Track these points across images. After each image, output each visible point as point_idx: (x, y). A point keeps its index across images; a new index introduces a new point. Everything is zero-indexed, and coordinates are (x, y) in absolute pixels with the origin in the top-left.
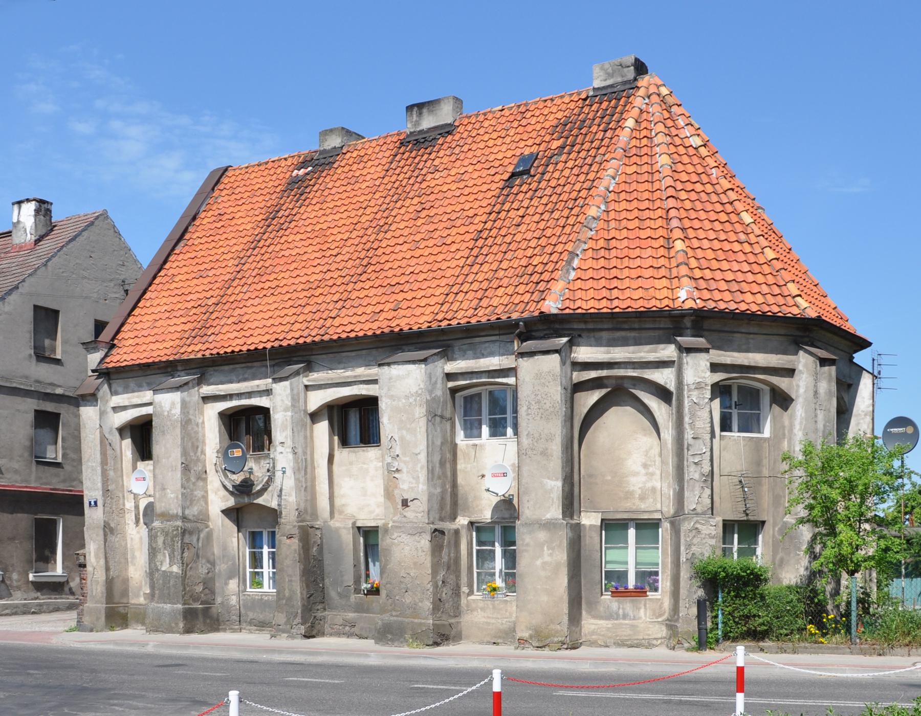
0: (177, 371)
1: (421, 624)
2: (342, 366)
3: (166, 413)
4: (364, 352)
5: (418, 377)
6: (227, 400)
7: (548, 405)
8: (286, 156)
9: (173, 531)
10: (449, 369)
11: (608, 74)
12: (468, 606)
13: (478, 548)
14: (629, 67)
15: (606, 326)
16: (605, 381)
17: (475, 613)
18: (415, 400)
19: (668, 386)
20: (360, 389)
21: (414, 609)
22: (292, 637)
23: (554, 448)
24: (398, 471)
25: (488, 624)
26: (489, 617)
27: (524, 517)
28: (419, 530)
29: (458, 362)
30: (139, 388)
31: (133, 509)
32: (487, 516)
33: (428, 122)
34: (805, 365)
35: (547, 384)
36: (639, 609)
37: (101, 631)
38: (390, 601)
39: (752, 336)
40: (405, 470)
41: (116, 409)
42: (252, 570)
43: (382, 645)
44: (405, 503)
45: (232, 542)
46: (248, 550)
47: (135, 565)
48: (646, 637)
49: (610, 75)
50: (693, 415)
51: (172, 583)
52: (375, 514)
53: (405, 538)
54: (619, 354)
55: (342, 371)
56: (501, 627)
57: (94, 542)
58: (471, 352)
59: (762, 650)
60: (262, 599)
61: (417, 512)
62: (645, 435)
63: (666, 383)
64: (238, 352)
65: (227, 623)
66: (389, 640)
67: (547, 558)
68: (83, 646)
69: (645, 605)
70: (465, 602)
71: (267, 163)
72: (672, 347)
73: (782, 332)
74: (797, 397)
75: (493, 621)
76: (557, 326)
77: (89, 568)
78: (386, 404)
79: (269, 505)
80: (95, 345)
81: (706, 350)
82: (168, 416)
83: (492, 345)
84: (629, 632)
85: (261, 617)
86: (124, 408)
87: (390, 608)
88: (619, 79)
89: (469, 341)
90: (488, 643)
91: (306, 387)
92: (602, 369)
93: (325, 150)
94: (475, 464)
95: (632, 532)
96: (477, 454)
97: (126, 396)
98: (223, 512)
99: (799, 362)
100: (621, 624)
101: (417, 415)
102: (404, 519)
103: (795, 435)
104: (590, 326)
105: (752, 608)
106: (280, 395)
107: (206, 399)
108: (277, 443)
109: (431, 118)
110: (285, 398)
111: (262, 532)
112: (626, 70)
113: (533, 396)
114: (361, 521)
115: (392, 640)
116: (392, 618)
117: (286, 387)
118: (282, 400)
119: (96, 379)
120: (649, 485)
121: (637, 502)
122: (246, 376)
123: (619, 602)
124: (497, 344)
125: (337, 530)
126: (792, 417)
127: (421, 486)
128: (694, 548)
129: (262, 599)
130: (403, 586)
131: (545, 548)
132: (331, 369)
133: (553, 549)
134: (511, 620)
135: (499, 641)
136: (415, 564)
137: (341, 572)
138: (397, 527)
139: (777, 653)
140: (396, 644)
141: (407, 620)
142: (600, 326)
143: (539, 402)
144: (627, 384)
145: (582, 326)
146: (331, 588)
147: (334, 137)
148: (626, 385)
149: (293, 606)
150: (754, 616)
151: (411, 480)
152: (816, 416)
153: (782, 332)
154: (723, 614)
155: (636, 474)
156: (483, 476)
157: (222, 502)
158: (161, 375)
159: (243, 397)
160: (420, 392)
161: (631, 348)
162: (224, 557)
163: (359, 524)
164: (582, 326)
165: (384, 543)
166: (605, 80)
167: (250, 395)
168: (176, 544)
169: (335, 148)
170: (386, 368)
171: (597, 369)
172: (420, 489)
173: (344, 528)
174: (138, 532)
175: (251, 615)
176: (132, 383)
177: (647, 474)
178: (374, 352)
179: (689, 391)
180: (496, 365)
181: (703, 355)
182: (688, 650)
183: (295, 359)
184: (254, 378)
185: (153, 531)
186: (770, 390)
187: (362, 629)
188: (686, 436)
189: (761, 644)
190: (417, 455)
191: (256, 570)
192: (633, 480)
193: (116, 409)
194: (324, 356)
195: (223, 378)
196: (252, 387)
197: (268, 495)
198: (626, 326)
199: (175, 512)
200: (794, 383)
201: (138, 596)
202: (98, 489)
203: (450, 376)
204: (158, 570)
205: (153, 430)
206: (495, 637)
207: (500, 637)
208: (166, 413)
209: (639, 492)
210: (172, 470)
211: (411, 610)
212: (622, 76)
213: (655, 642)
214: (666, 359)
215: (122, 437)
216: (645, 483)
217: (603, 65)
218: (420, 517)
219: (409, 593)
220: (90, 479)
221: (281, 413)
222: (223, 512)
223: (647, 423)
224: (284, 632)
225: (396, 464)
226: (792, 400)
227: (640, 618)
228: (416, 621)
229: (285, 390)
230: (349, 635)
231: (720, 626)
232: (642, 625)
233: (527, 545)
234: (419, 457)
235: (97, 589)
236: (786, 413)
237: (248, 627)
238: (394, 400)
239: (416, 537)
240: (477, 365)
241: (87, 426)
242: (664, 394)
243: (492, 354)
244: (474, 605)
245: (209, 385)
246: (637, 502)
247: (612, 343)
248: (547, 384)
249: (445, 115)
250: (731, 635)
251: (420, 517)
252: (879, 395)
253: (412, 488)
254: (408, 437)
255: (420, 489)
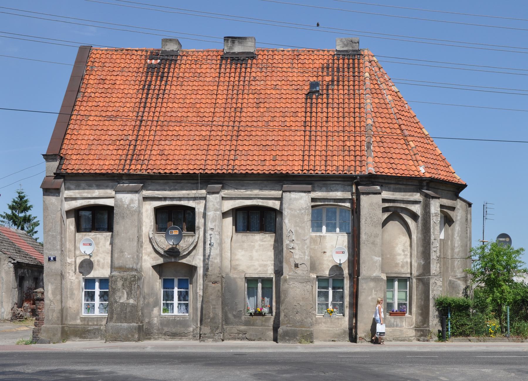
0: (123, 180)
1: (306, 331)
2: (244, 188)
3: (126, 206)
4: (259, 182)
5: (307, 200)
6: (162, 201)
7: (375, 220)
8: (137, 49)
9: (131, 278)
10: (314, 196)
11: (345, 44)
12: (316, 321)
13: (319, 290)
14: (356, 43)
15: (393, 182)
16: (390, 209)
17: (320, 325)
18: (305, 212)
19: (417, 213)
20: (257, 202)
21: (302, 323)
22: (216, 341)
23: (378, 241)
24: (293, 248)
25: (329, 330)
26: (328, 327)
27: (362, 274)
28: (306, 280)
29: (317, 192)
30: (107, 187)
31: (73, 263)
32: (326, 273)
33: (238, 49)
34: (461, 206)
35: (375, 209)
36: (403, 322)
37: (58, 342)
38: (286, 318)
39: (443, 191)
40: (297, 248)
41: (67, 199)
42: (165, 302)
43: (283, 343)
44: (296, 266)
45: (156, 285)
46: (162, 290)
47: (73, 299)
48: (407, 336)
49: (346, 45)
50: (434, 228)
51: (128, 310)
52: (258, 270)
53: (297, 284)
54: (398, 196)
55: (244, 190)
56: (336, 332)
57: (52, 284)
58: (325, 188)
59: (470, 340)
60: (175, 319)
61: (303, 271)
62: (403, 236)
63: (417, 212)
64: (174, 174)
65: (152, 334)
66: (287, 340)
67: (374, 296)
68: (94, 351)
69: (405, 320)
70: (315, 319)
71: (122, 50)
72: (418, 195)
73: (452, 190)
74: (456, 221)
75: (331, 329)
76: (373, 180)
77: (46, 301)
78: (288, 212)
79: (190, 264)
80: (55, 157)
81: (439, 198)
82: (128, 207)
83: (337, 186)
84: (400, 334)
85: (174, 330)
86: (75, 199)
87: (286, 322)
88: (351, 49)
89: (324, 182)
90: (329, 341)
91: (222, 197)
92: (390, 203)
93: (166, 51)
94: (320, 246)
95: (396, 283)
96: (321, 241)
97: (77, 191)
98: (154, 267)
99: (457, 204)
100: (396, 329)
101: (306, 220)
102: (295, 274)
103: (455, 238)
104: (387, 181)
105: (465, 320)
106: (212, 201)
107: (146, 199)
108: (209, 229)
109: (240, 47)
110: (215, 204)
111: (173, 279)
112: (354, 44)
113: (368, 215)
114: (249, 274)
115: (289, 340)
116: (288, 328)
117: (217, 197)
118: (214, 205)
119: (54, 179)
120: (405, 260)
121: (400, 268)
122: (176, 187)
123: (394, 319)
124: (340, 185)
125: (235, 279)
126: (453, 231)
127: (306, 257)
128: (434, 292)
129: (175, 319)
130: (295, 310)
131: (373, 291)
132: (237, 189)
133: (377, 291)
134: (341, 328)
135: (335, 339)
136: (303, 298)
137: (236, 303)
138: (292, 279)
139: (477, 342)
140: (291, 342)
141: (298, 329)
142: (390, 182)
143: (371, 218)
144: (399, 211)
145: (383, 181)
146: (228, 312)
147: (172, 44)
148: (398, 211)
149: (216, 323)
150: (466, 325)
151: (301, 253)
152: (467, 230)
153: (452, 190)
154: (451, 324)
155: (400, 255)
156: (324, 252)
157: (153, 260)
158: (109, 181)
159: (175, 200)
160: (308, 208)
161: (403, 193)
162: (152, 294)
163: (247, 276)
164: (383, 181)
165: (284, 287)
166: (343, 47)
167: (180, 199)
168: (133, 286)
169: (173, 51)
170: (288, 193)
171: (388, 202)
172: (306, 259)
173: (239, 278)
174: (77, 278)
175: (166, 329)
176: (83, 184)
177: (404, 255)
178: (265, 182)
179: (433, 217)
180: (340, 196)
181: (437, 200)
182: (435, 341)
183: (213, 181)
184: (182, 189)
185: (114, 278)
186: (444, 216)
187: (251, 335)
188: (431, 238)
189: (469, 338)
190: (305, 240)
191: (168, 302)
192: (398, 257)
193: (67, 199)
194: (233, 181)
195: (158, 187)
196: (183, 194)
197: (190, 257)
198: (401, 183)
199: (131, 266)
200: (454, 214)
201: (75, 319)
202: (57, 250)
203: (313, 200)
204: (116, 302)
205: (115, 215)
206: (333, 337)
207: (336, 337)
208: (126, 206)
209: (401, 263)
210: (130, 241)
211: (299, 323)
212: (352, 47)
213: (411, 338)
214: (418, 200)
215: (68, 217)
216: (403, 259)
217: (342, 39)
218: (305, 273)
219: (299, 314)
220: (50, 243)
221: (213, 212)
222: (154, 267)
223: (404, 230)
224: (209, 338)
225: (292, 245)
226: (453, 222)
227: (403, 326)
228: (303, 329)
229: (215, 199)
230: (242, 339)
231: (449, 330)
232: (405, 330)
233: (364, 289)
234: (306, 242)
235: (53, 315)
236: (450, 228)
237: (163, 337)
238: (292, 211)
239: (304, 284)
240: (328, 195)
241: (49, 209)
242: (414, 216)
243: (337, 190)
244: (320, 321)
245: (147, 190)
246: (400, 268)
247: (395, 190)
248: (375, 209)
249: (249, 47)
250: (455, 334)
251: (305, 273)
252: (486, 222)
253: (301, 258)
254: (300, 231)
255: (306, 259)
